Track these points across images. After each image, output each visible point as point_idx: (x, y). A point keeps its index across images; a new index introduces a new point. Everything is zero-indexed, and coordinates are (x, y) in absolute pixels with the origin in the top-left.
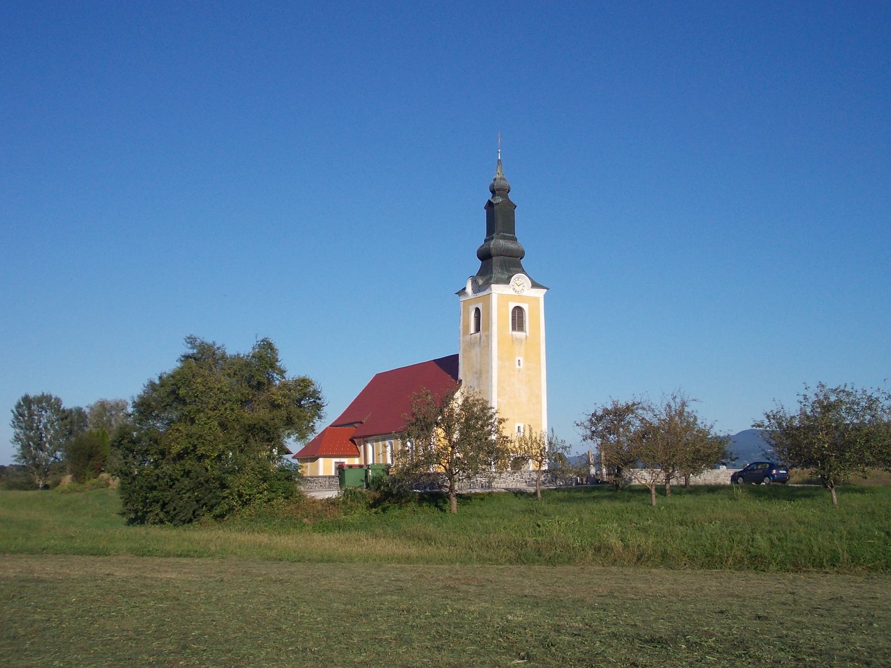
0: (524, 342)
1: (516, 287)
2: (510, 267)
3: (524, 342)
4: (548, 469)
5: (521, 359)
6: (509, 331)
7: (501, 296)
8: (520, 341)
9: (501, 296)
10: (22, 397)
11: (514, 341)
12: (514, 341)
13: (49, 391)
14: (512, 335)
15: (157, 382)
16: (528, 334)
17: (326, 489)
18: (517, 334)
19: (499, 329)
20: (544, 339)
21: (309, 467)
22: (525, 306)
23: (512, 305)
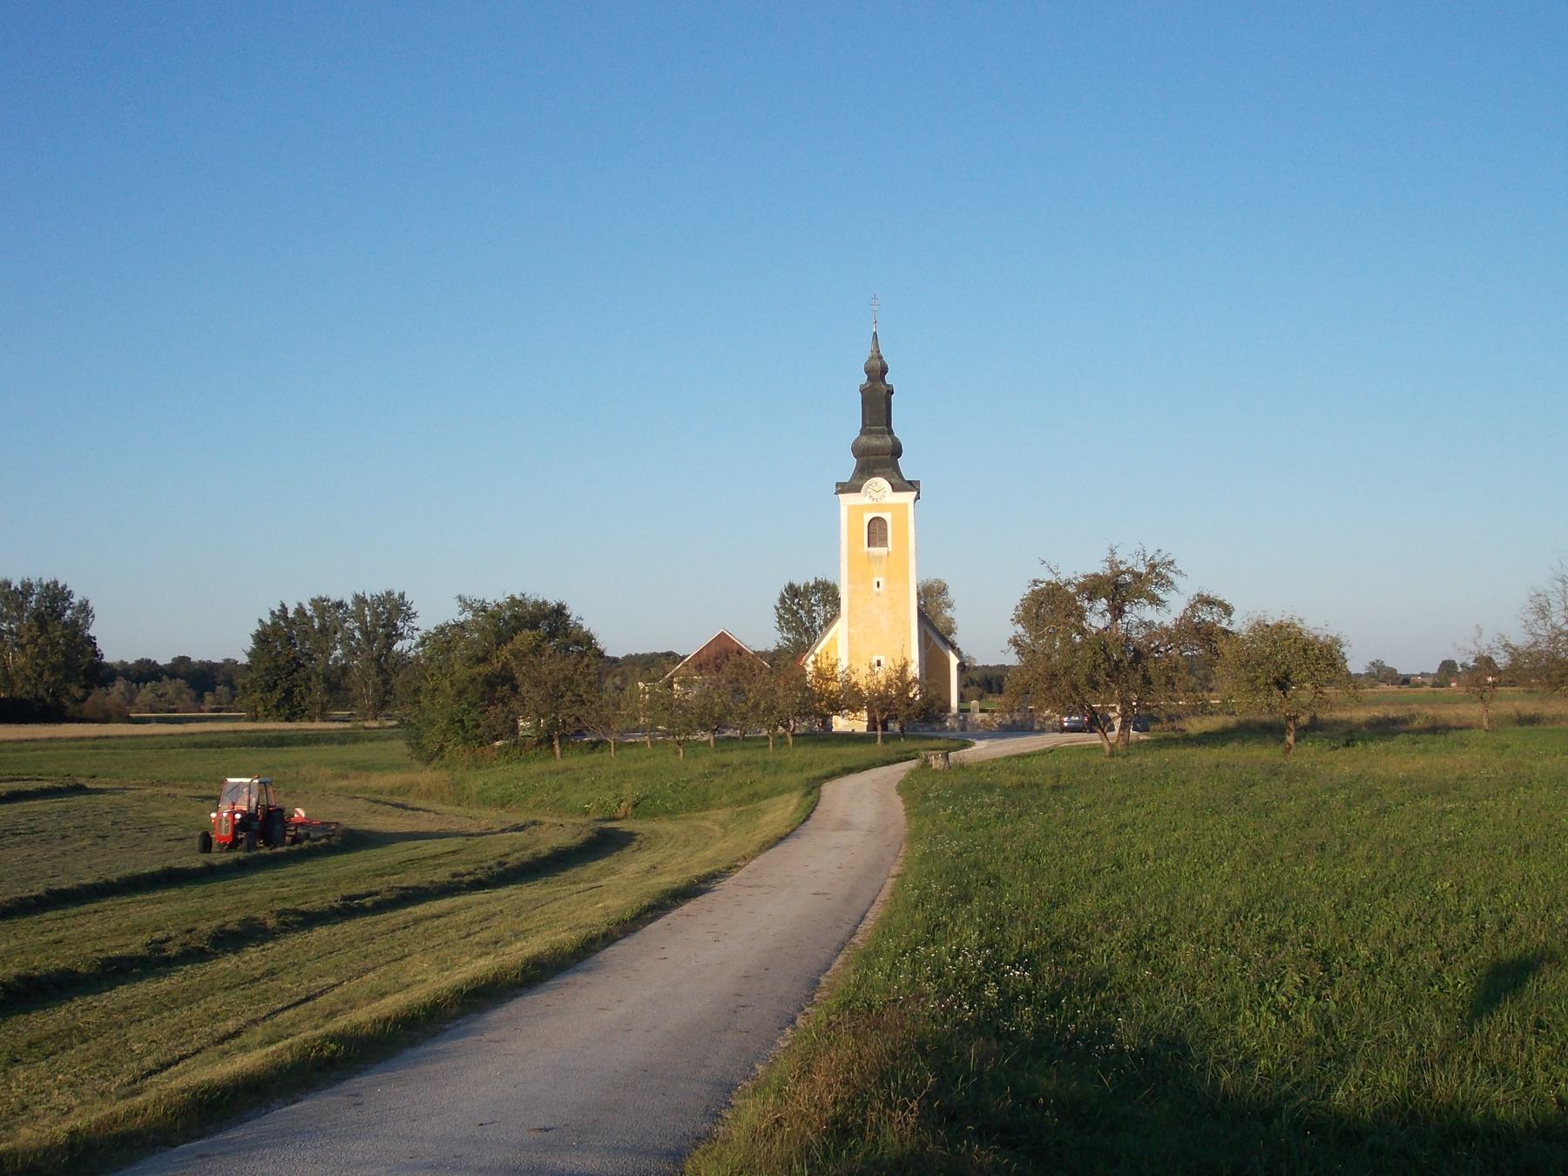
0: (885, 559)
1: (875, 495)
2: (874, 468)
3: (885, 559)
4: (251, 662)
5: (881, 580)
6: (863, 548)
7: (851, 508)
8: (879, 558)
9: (851, 508)
10: (1336, 641)
11: (870, 559)
12: (870, 559)
13: (1498, 634)
14: (868, 552)
15: (396, 596)
16: (890, 549)
17: (893, 747)
18: (878, 551)
19: (849, 547)
20: (842, 559)
21: (1094, 738)
22: (887, 516)
23: (868, 517)
